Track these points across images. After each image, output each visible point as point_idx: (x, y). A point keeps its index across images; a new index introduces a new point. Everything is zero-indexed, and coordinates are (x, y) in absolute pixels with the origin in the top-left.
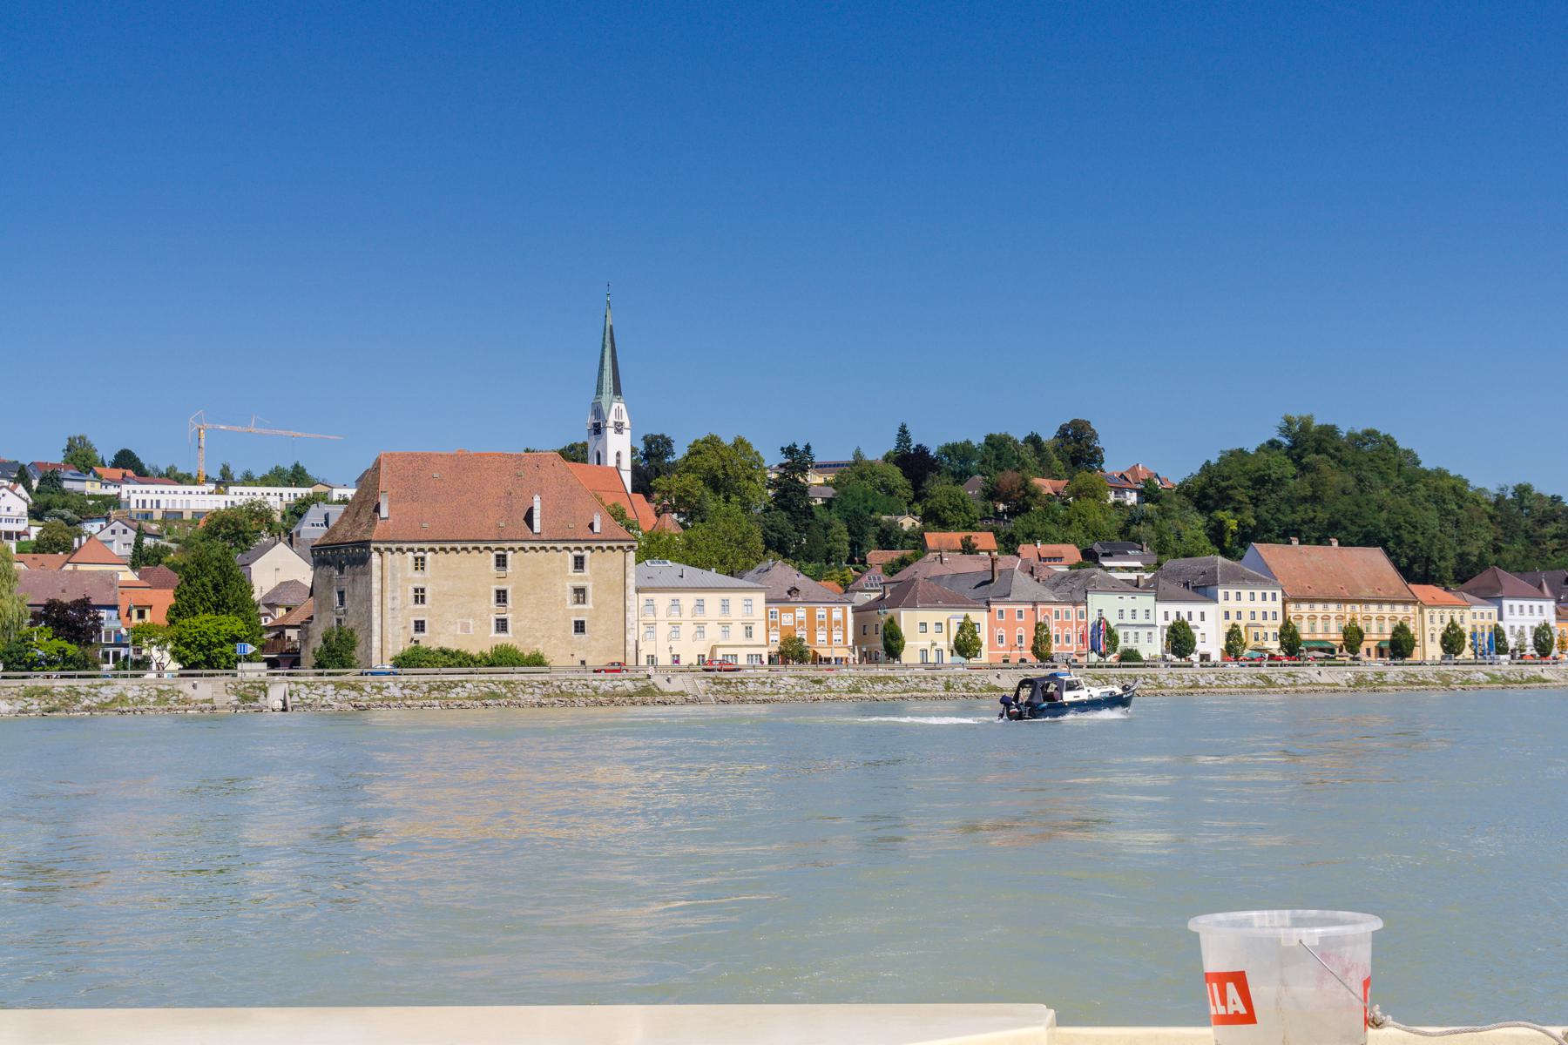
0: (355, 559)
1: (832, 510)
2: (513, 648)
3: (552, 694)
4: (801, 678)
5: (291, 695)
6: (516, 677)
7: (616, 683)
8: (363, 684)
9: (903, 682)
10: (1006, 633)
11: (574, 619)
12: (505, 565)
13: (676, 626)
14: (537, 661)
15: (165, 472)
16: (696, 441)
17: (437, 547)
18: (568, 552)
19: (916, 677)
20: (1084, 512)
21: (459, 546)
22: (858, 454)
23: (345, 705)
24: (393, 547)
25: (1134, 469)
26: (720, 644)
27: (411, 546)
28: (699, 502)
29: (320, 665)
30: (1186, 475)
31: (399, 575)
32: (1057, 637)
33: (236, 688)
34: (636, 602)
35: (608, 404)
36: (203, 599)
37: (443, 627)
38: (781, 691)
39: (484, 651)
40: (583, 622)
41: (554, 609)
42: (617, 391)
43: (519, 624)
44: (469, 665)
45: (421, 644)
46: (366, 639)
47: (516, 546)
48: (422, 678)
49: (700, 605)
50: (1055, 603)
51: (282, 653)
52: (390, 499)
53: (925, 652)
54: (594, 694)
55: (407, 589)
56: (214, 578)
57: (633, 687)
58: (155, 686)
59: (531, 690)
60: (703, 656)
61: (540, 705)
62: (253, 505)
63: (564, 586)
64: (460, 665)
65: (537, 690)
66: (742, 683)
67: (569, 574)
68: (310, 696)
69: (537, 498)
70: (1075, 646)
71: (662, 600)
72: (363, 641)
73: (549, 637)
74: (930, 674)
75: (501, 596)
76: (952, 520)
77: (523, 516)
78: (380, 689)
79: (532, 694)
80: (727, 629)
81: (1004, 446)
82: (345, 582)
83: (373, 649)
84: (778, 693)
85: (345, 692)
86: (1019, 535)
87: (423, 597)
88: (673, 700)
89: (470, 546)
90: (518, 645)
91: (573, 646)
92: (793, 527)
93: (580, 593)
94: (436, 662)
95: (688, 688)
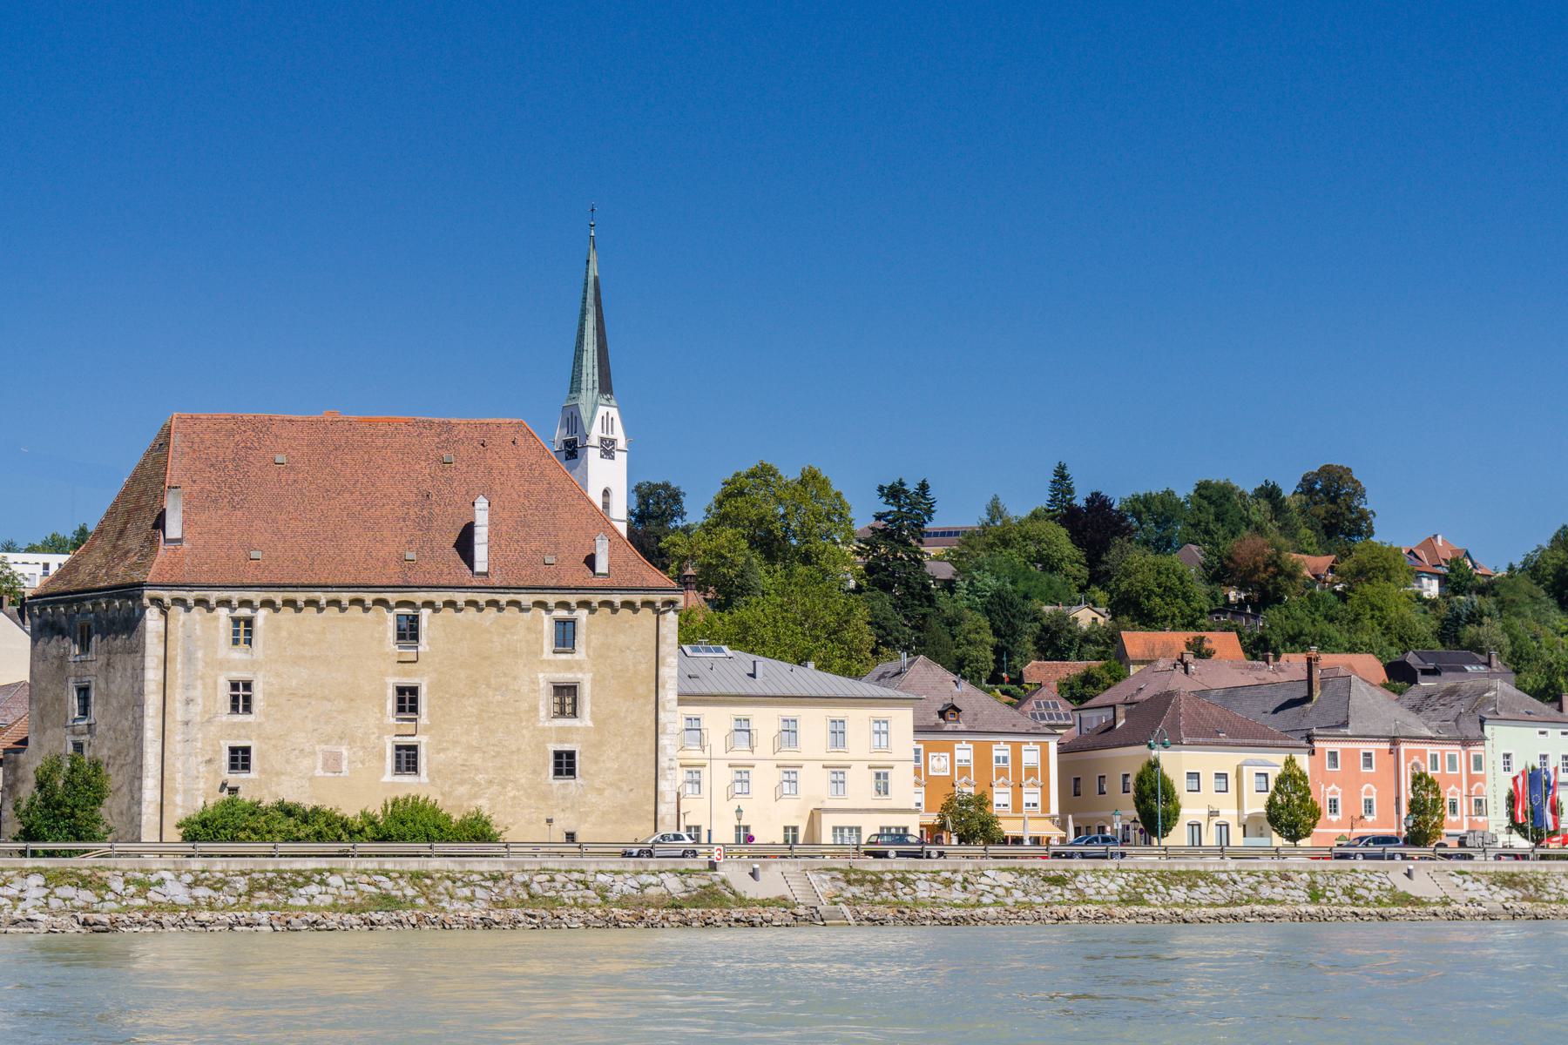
0: (112, 622)
2: (428, 805)
3: (511, 901)
4: (1022, 872)
6: (434, 864)
7: (645, 879)
8: (107, 874)
9: (1226, 883)
10: (1343, 794)
13: (742, 772)
14: (478, 832)
16: (737, 475)
17: (278, 597)
18: (543, 612)
19: (1250, 874)
20: (1380, 603)
21: (323, 597)
22: (995, 510)
23: (64, 920)
24: (190, 596)
25: (1429, 544)
26: (828, 805)
27: (225, 595)
28: (741, 575)
29: (28, 835)
30: (1530, 549)
31: (200, 654)
32: (1453, 806)
34: (674, 716)
37: (288, 761)
38: (985, 900)
39: (370, 810)
40: (571, 755)
41: (512, 727)
42: (606, 387)
43: (442, 755)
44: (339, 839)
45: (241, 795)
46: (131, 783)
47: (439, 597)
48: (235, 865)
49: (790, 730)
50: (1431, 740)
52: (187, 503)
53: (1196, 828)
54: (599, 901)
57: (681, 887)
59: (467, 892)
60: (795, 829)
61: (487, 924)
63: (534, 682)
64: (319, 837)
65: (480, 893)
66: (903, 880)
67: (545, 656)
69: (482, 503)
70: (1466, 820)
71: (717, 720)
72: (125, 789)
73: (503, 784)
74: (1276, 868)
75: (407, 699)
76: (1163, 613)
77: (453, 540)
78: (144, 887)
79: (470, 900)
80: (841, 777)
81: (1228, 499)
82: (92, 668)
83: (144, 805)
84: (979, 904)
85: (69, 891)
86: (1275, 639)
87: (247, 699)
88: (768, 916)
89: (345, 597)
90: (440, 799)
91: (551, 803)
93: (566, 695)
95: (797, 892)
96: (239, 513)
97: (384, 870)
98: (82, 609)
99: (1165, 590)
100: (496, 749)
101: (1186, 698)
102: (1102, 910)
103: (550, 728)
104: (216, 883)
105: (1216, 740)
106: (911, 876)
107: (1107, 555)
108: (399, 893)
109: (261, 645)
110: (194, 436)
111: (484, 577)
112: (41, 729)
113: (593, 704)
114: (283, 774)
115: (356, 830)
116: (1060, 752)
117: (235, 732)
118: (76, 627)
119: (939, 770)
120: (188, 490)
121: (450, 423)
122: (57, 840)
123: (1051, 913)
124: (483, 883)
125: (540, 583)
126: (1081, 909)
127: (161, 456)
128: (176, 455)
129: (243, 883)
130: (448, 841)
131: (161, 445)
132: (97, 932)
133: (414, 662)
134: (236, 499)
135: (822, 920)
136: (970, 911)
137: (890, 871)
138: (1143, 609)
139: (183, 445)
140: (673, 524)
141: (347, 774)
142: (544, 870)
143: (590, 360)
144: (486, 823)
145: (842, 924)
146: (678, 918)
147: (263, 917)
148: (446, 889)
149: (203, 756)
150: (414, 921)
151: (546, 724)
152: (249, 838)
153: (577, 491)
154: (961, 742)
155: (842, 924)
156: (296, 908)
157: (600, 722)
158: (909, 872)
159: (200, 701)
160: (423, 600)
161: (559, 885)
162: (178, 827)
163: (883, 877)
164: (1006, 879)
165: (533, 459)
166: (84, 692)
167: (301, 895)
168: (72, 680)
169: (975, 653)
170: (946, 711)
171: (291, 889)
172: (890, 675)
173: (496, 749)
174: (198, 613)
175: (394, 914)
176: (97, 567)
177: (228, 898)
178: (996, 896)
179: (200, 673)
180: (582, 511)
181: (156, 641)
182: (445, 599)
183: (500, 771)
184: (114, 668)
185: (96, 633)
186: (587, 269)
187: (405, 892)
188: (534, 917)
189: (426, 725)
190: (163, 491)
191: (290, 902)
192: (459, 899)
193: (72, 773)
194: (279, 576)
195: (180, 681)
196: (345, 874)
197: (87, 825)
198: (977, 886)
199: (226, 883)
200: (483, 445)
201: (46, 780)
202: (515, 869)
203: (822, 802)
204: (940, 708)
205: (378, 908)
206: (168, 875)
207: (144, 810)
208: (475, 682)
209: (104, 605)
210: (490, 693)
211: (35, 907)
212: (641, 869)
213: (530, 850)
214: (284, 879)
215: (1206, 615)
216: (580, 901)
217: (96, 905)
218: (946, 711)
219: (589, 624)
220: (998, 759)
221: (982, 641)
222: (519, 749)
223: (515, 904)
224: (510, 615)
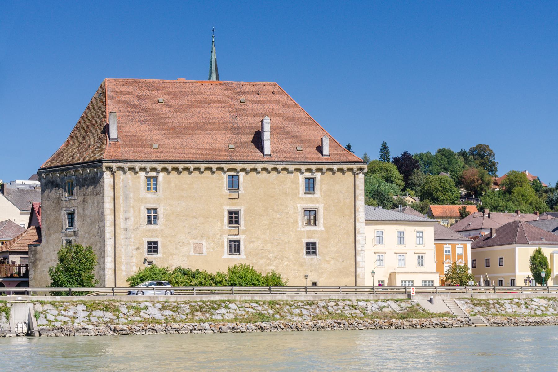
0: (85, 180)
5: (37, 317)
7: (381, 304)
8: (118, 304)
17: (170, 166)
18: (299, 174)
21: (191, 166)
23: (102, 328)
24: (126, 166)
26: (397, 271)
27: (143, 165)
29: (56, 284)
31: (131, 195)
37: (176, 248)
40: (314, 244)
43: (252, 244)
44: (211, 285)
47: (249, 166)
51: (7, 277)
55: (140, 210)
57: (399, 308)
59: (298, 311)
63: (296, 208)
64: (201, 284)
65: (305, 312)
66: (498, 304)
73: (282, 259)
77: (251, 139)
78: (138, 310)
80: (402, 258)
82: (75, 203)
83: (106, 270)
85: (99, 313)
89: (203, 166)
94: (176, 283)
96: (145, 126)
97: (255, 300)
98: (68, 174)
99: (443, 189)
100: (278, 242)
101: (524, 224)
103: (304, 231)
104: (173, 308)
105: (542, 242)
107: (411, 177)
108: (266, 312)
109: (161, 190)
111: (269, 157)
116: (472, 248)
117: (150, 234)
118: (65, 183)
121: (241, 84)
124: (305, 307)
125: (297, 160)
128: (109, 98)
131: (101, 94)
132: (123, 335)
133: (237, 199)
135: (473, 323)
138: (434, 197)
142: (331, 300)
146: (408, 324)
147: (206, 325)
151: (302, 229)
159: (132, 218)
160: (241, 168)
164: (543, 302)
166: (71, 215)
171: (212, 310)
173: (278, 242)
174: (130, 174)
176: (74, 154)
179: (131, 205)
181: (109, 188)
184: (87, 202)
185: (77, 185)
186: (212, 55)
187: (269, 312)
191: (213, 317)
192: (296, 315)
193: (77, 253)
198: (532, 306)
200: (258, 94)
203: (395, 269)
206: (148, 304)
207: (106, 273)
209: (81, 171)
210: (275, 214)
213: (295, 290)
215: (459, 199)
220: (446, 251)
222: (289, 242)
224: (283, 175)
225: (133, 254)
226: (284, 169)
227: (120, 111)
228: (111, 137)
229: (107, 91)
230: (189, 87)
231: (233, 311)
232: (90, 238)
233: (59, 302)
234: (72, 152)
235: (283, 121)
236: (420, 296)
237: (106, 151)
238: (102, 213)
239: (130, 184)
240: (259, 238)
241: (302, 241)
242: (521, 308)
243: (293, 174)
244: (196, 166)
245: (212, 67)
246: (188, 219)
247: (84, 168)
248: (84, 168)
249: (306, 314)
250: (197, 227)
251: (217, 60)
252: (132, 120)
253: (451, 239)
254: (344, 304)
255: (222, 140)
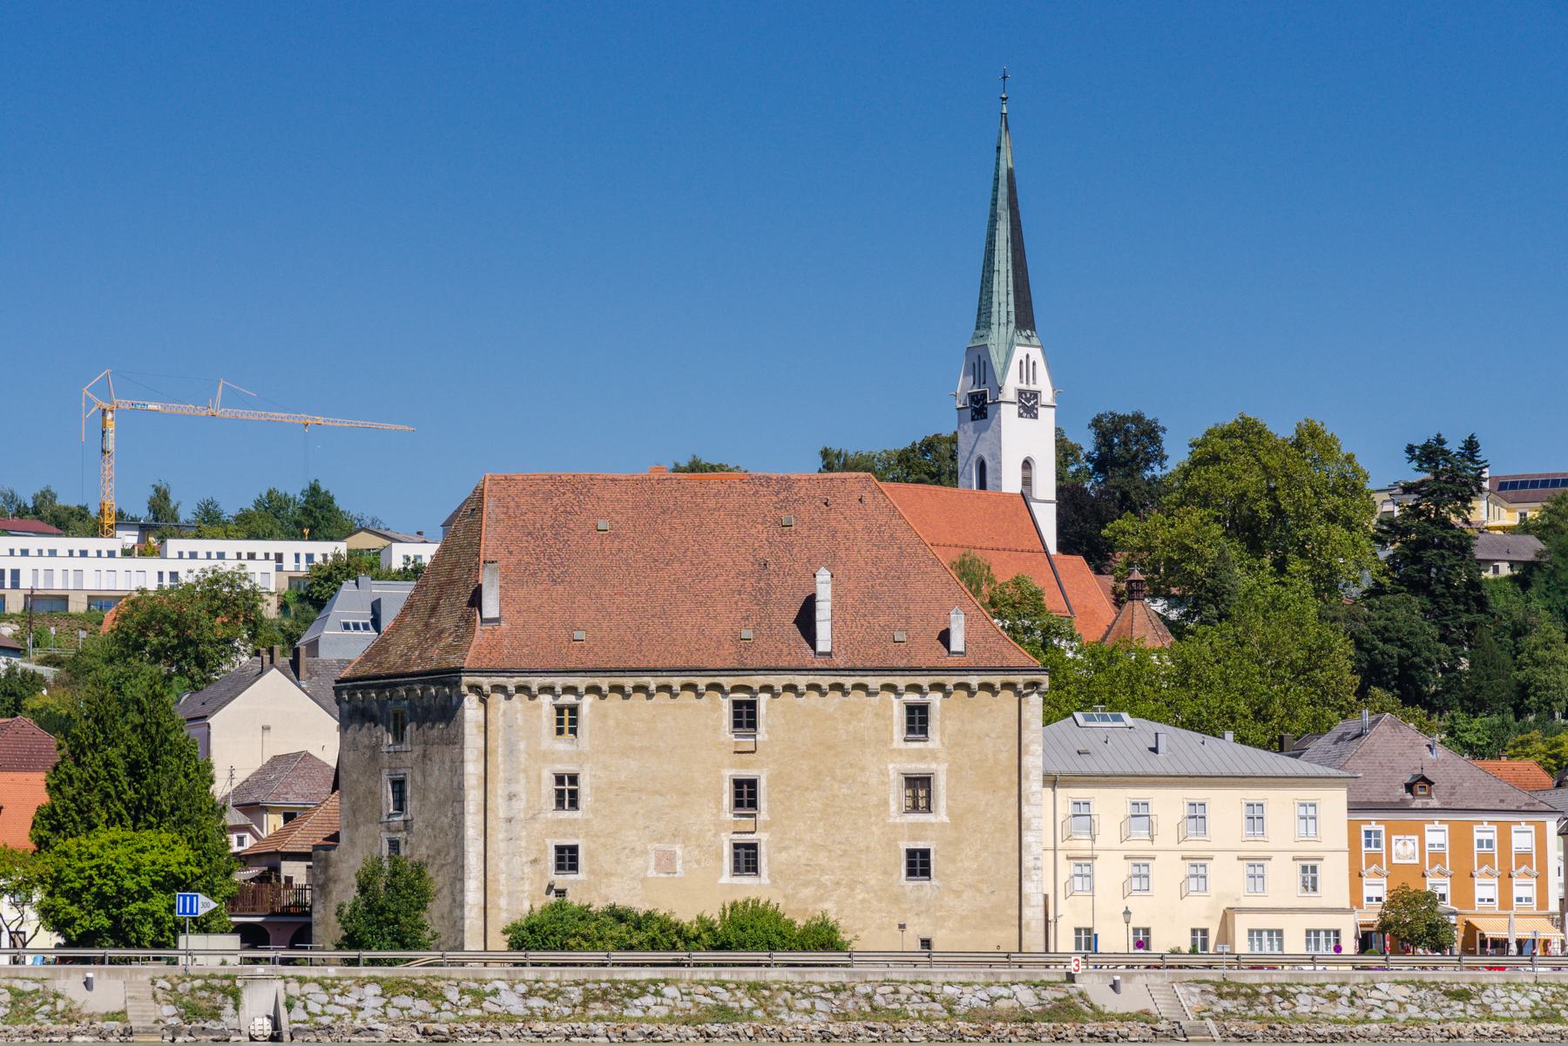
0: (427, 710)
1: (1533, 591)
2: (770, 909)
5: (289, 1006)
6: (773, 975)
7: (996, 991)
8: (442, 983)
11: (905, 845)
12: (753, 724)
13: (1141, 870)
15: (30, 505)
17: (604, 683)
18: (892, 696)
21: (652, 682)
23: (403, 1029)
24: (511, 683)
26: (1245, 903)
27: (547, 681)
29: (352, 941)
31: (522, 746)
33: (174, 989)
35: (1003, 349)
36: (108, 795)
37: (618, 861)
38: (1373, 1016)
39: (707, 915)
40: (925, 853)
41: (861, 823)
42: (1025, 319)
43: (783, 854)
44: (674, 947)
45: (569, 899)
46: (452, 884)
47: (778, 681)
48: (569, 974)
49: (1197, 815)
51: (274, 914)
54: (945, 1014)
55: (539, 777)
56: (129, 748)
57: (1035, 1000)
58: (6, 982)
59: (806, 1004)
60: (1205, 932)
62: (217, 581)
63: (884, 773)
64: (654, 945)
65: (820, 1005)
66: (1283, 994)
67: (894, 745)
68: (330, 1009)
69: (824, 576)
72: (446, 892)
73: (852, 886)
75: (745, 794)
78: (479, 997)
79: (809, 1012)
80: (1259, 871)
82: (408, 759)
83: (467, 909)
84: (1367, 1019)
87: (573, 794)
88: (1124, 1031)
89: (676, 682)
90: (782, 902)
91: (905, 906)
92: (1434, 631)
93: (919, 787)
94: (601, 939)
96: (560, 588)
97: (721, 981)
98: (394, 696)
100: (843, 847)
102: (1502, 1027)
103: (902, 825)
104: (550, 993)
106: (1291, 990)
108: (736, 1005)
109: (586, 734)
110: (509, 499)
111: (827, 658)
112: (354, 826)
113: (948, 797)
114: (612, 875)
115: (692, 936)
117: (561, 829)
118: (388, 714)
119: (1406, 857)
120: (504, 562)
122: (379, 949)
123: (1442, 1030)
124: (823, 995)
125: (888, 664)
126: (1478, 1026)
127: (473, 522)
129: (577, 993)
130: (790, 950)
131: (473, 510)
133: (752, 752)
134: (557, 572)
135: (1185, 1036)
136: (1349, 1028)
137: (1269, 984)
139: (497, 510)
140: (1149, 473)
141: (682, 875)
142: (888, 981)
143: (1003, 284)
144: (833, 930)
145: (1207, 1041)
146: (1027, 1032)
147: (599, 1028)
148: (785, 1001)
149: (528, 855)
150: (750, 1033)
151: (898, 820)
152: (580, 945)
153: (931, 556)
154: (1432, 822)
155: (1207, 1041)
156: (631, 1019)
157: (957, 818)
158: (1290, 985)
159: (523, 796)
160: (761, 684)
161: (903, 998)
162: (505, 932)
163: (1259, 990)
164: (1401, 993)
165: (882, 519)
167: (636, 1006)
168: (385, 772)
169: (1543, 677)
170: (1415, 783)
171: (626, 999)
172: (1349, 737)
174: (519, 700)
175: (731, 1027)
176: (409, 649)
177: (563, 1008)
178: (1387, 1011)
179: (522, 767)
180: (937, 580)
181: (475, 731)
182: (785, 683)
183: (848, 872)
184: (430, 760)
185: (411, 721)
186: (998, 159)
188: (874, 1030)
189: (765, 822)
190: (477, 564)
192: (798, 1011)
194: (605, 659)
195: (501, 774)
196: (680, 985)
197: (412, 931)
198: (1367, 1001)
199: (560, 993)
200: (826, 504)
201: (369, 884)
202: (857, 980)
203: (1237, 900)
204: (1408, 779)
205: (715, 1020)
208: (819, 773)
210: (836, 786)
211: (373, 1016)
212: (993, 981)
214: (618, 989)
216: (925, 1013)
217: (433, 1016)
218: (1415, 783)
219: (944, 709)
220: (1480, 843)
221: (1553, 660)
222: (868, 848)
223: (857, 1017)
224: (856, 699)
225: (523, 873)
226: (857, 687)
227: (511, 553)
228: (486, 615)
229: (485, 505)
230: (671, 491)
231: (670, 1002)
232: (435, 836)
233: (332, 979)
234: (406, 644)
235: (874, 570)
236: (1096, 976)
237: (472, 648)
238: (459, 783)
239: (520, 722)
240: (800, 840)
241: (897, 846)
242: (1335, 1005)
243: (878, 697)
244: (663, 681)
245: (999, 196)
246: (644, 797)
247: (426, 685)
248: (426, 685)
249: (824, 1009)
250: (664, 814)
251: (1016, 175)
252: (533, 575)
253: (1498, 808)
254: (911, 991)
255: (728, 617)
